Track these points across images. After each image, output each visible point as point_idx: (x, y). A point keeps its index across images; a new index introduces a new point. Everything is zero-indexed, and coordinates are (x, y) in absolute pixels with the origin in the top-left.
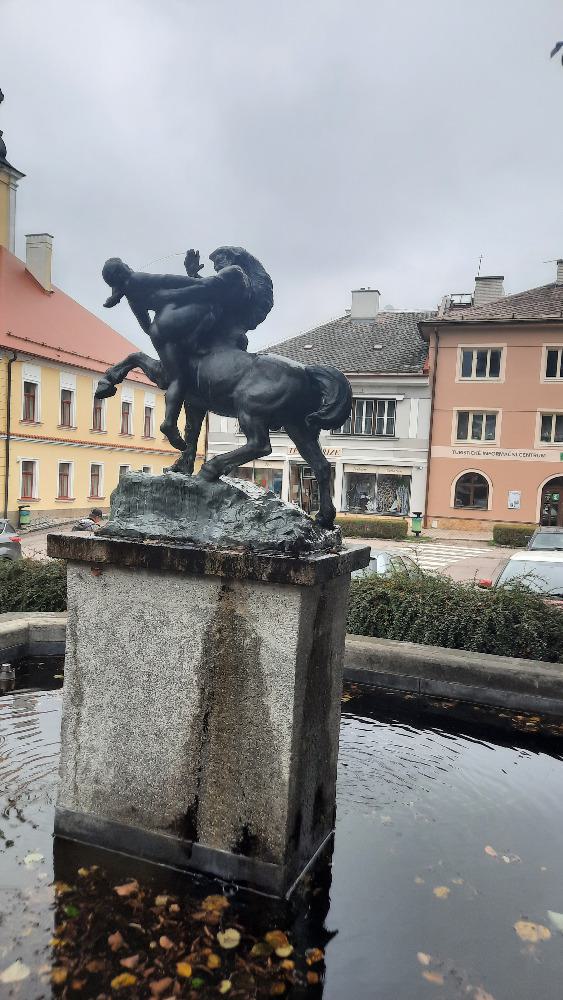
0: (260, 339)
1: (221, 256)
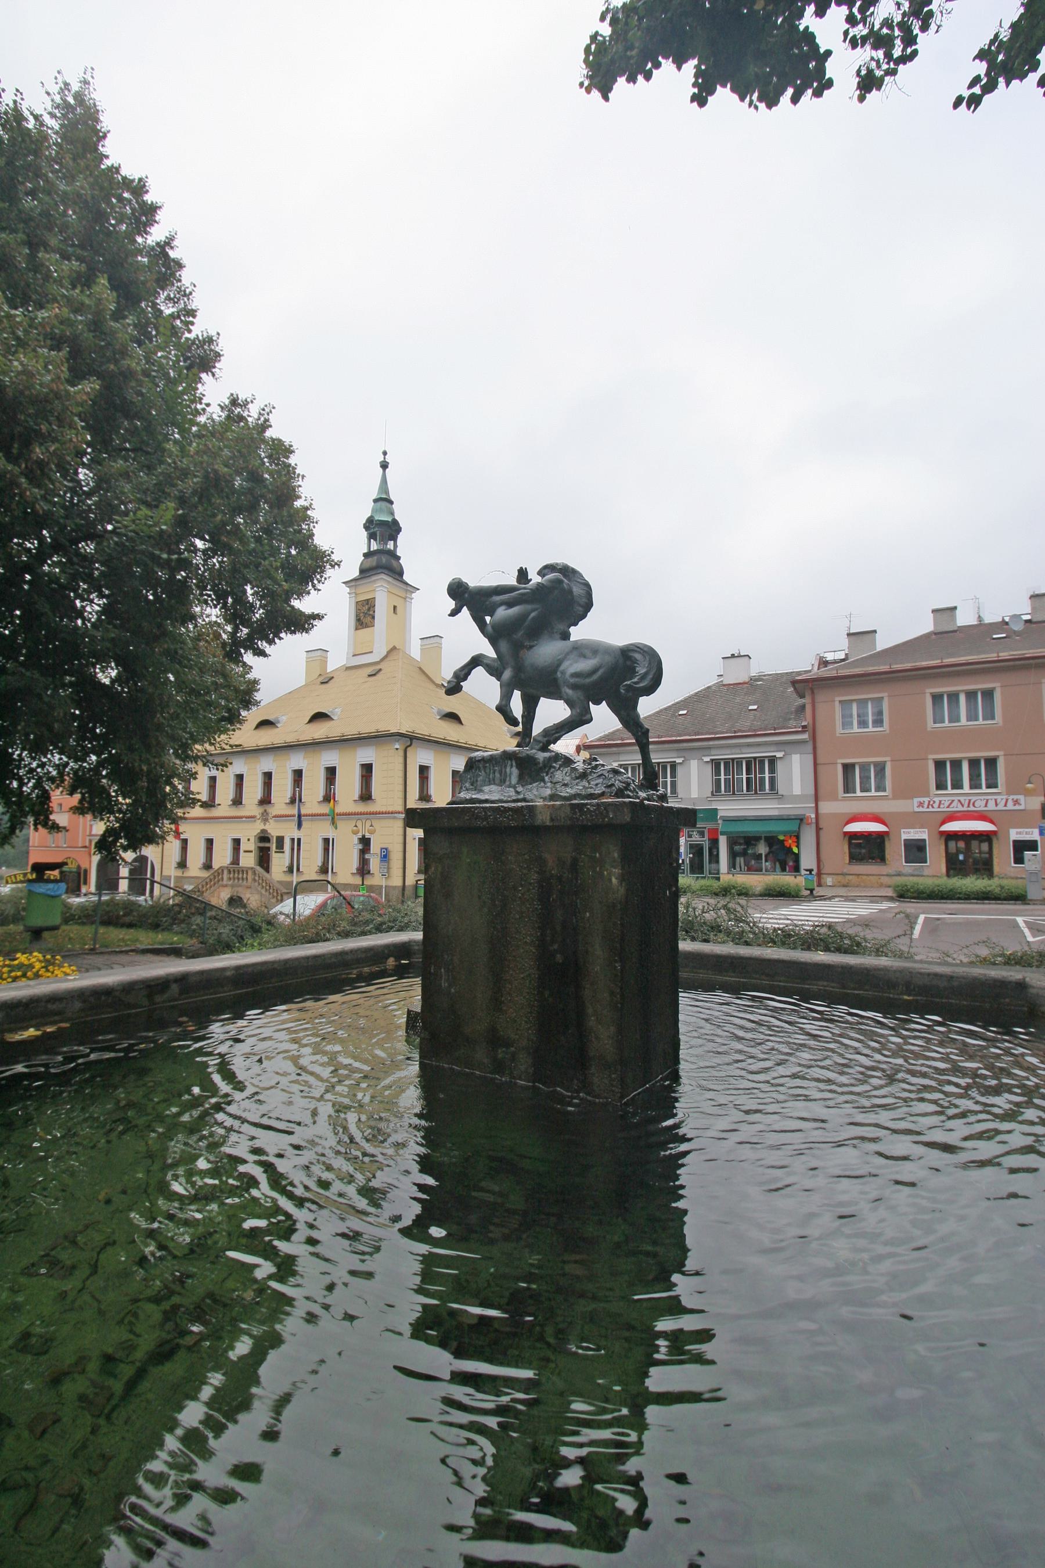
0: (578, 633)
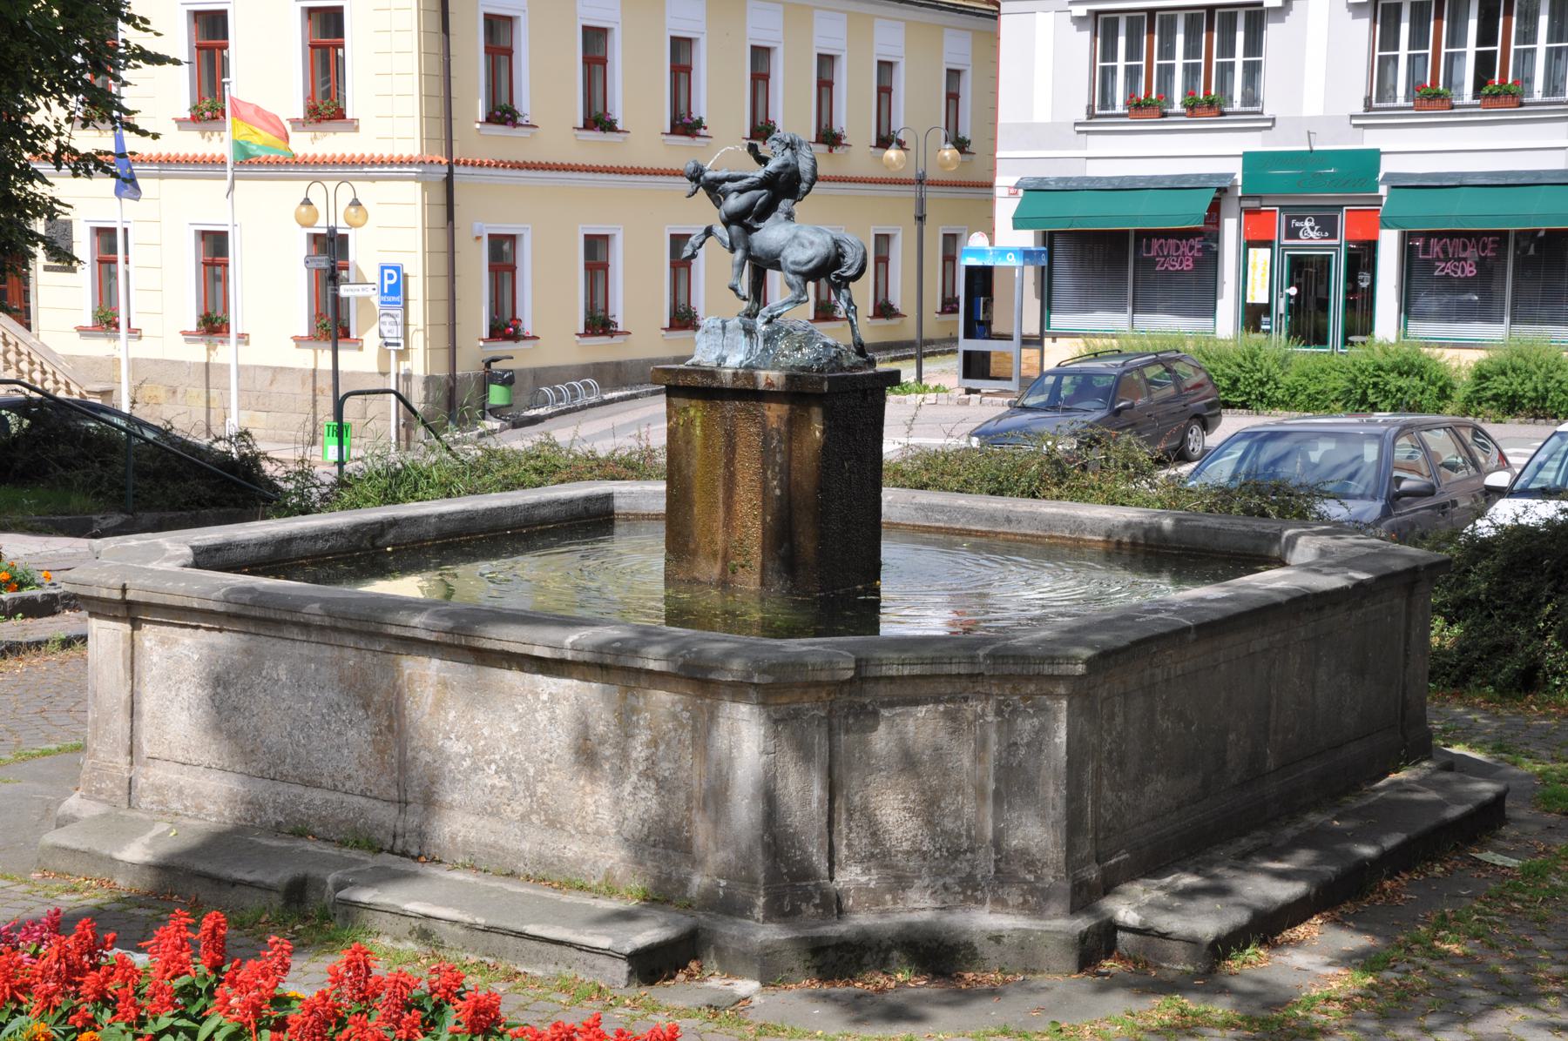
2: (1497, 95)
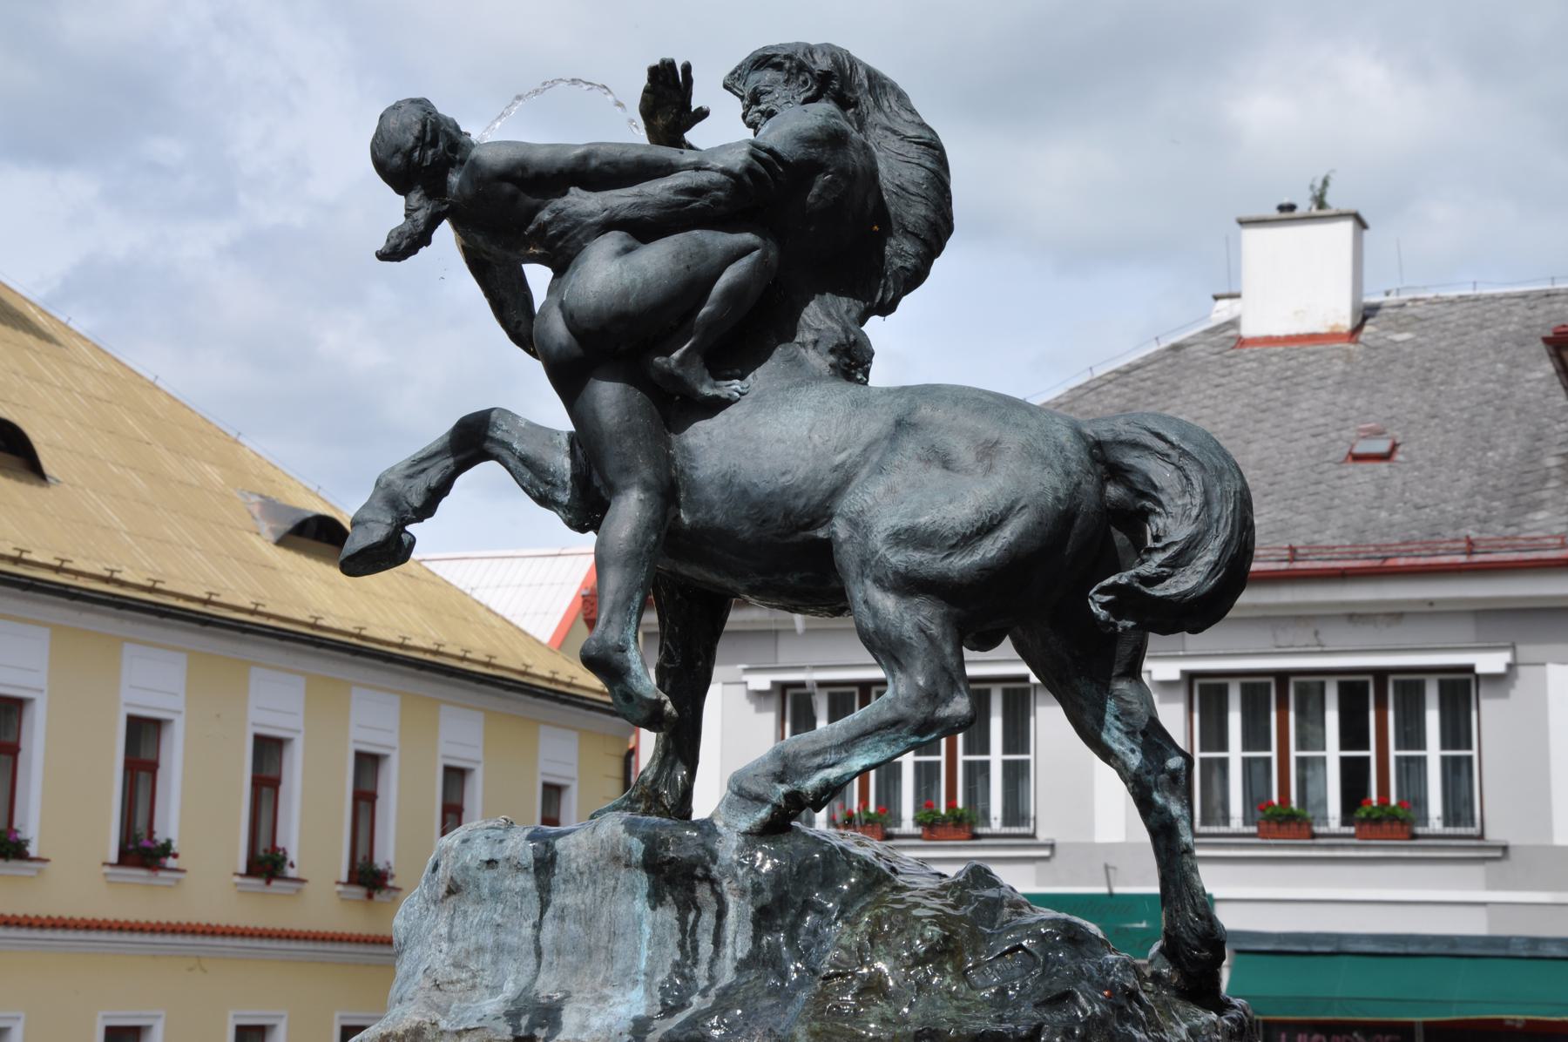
0: (909, 343)
1: (770, 71)
2: (1378, 821)
